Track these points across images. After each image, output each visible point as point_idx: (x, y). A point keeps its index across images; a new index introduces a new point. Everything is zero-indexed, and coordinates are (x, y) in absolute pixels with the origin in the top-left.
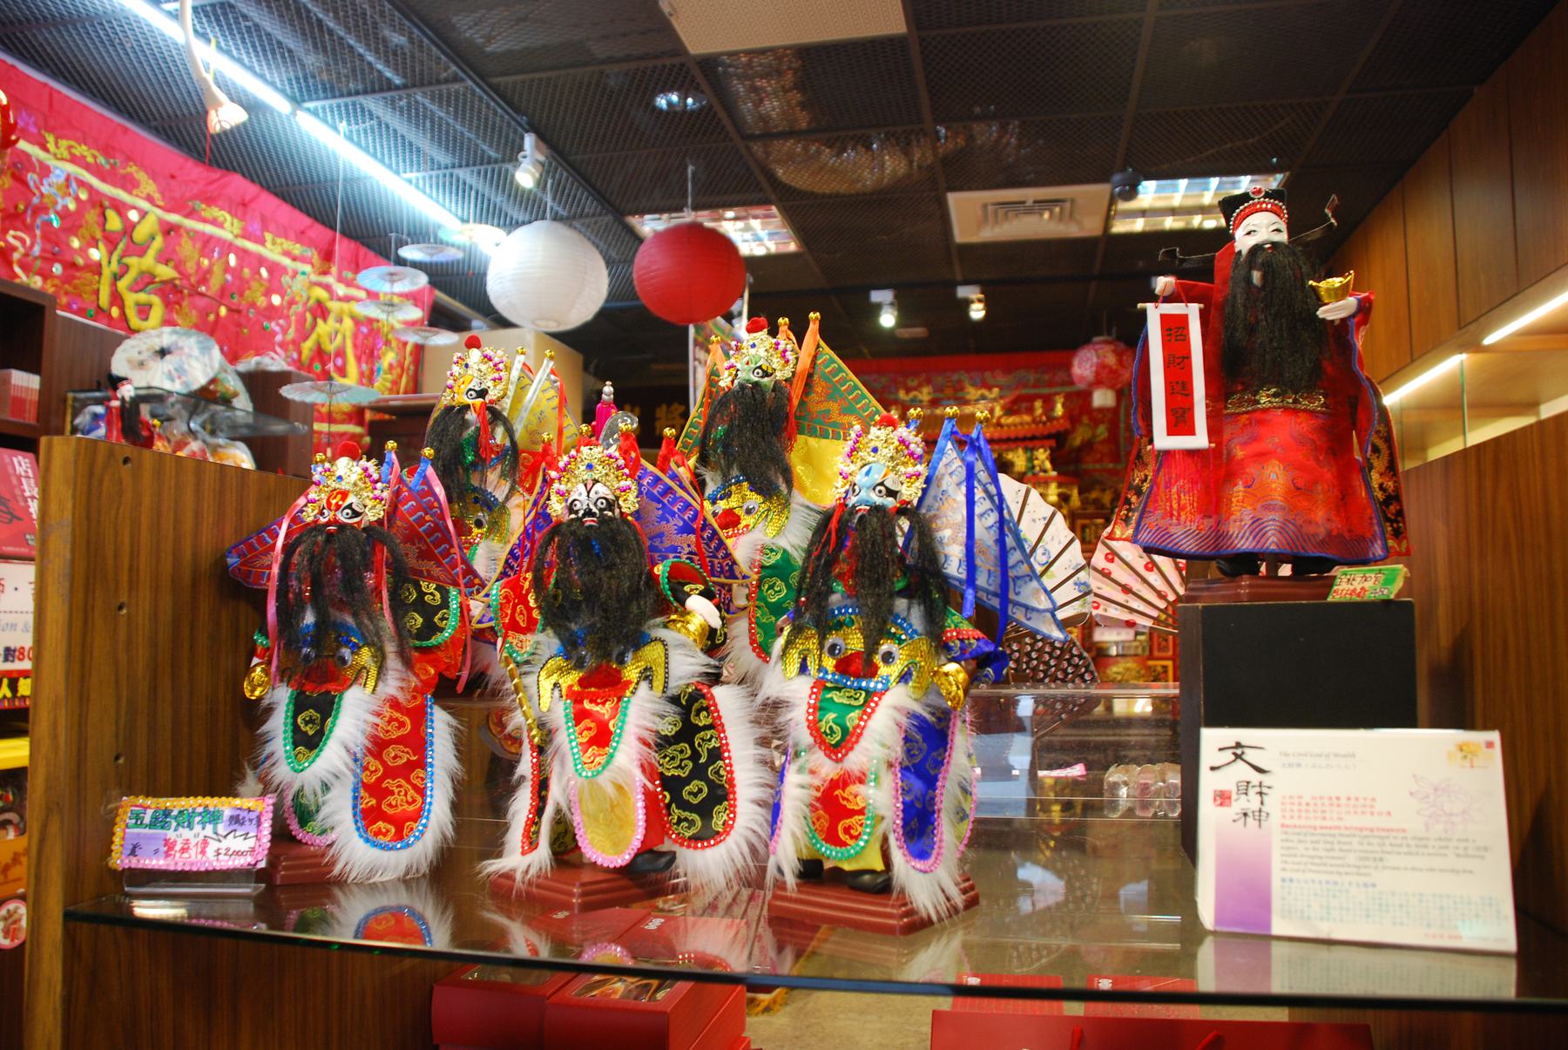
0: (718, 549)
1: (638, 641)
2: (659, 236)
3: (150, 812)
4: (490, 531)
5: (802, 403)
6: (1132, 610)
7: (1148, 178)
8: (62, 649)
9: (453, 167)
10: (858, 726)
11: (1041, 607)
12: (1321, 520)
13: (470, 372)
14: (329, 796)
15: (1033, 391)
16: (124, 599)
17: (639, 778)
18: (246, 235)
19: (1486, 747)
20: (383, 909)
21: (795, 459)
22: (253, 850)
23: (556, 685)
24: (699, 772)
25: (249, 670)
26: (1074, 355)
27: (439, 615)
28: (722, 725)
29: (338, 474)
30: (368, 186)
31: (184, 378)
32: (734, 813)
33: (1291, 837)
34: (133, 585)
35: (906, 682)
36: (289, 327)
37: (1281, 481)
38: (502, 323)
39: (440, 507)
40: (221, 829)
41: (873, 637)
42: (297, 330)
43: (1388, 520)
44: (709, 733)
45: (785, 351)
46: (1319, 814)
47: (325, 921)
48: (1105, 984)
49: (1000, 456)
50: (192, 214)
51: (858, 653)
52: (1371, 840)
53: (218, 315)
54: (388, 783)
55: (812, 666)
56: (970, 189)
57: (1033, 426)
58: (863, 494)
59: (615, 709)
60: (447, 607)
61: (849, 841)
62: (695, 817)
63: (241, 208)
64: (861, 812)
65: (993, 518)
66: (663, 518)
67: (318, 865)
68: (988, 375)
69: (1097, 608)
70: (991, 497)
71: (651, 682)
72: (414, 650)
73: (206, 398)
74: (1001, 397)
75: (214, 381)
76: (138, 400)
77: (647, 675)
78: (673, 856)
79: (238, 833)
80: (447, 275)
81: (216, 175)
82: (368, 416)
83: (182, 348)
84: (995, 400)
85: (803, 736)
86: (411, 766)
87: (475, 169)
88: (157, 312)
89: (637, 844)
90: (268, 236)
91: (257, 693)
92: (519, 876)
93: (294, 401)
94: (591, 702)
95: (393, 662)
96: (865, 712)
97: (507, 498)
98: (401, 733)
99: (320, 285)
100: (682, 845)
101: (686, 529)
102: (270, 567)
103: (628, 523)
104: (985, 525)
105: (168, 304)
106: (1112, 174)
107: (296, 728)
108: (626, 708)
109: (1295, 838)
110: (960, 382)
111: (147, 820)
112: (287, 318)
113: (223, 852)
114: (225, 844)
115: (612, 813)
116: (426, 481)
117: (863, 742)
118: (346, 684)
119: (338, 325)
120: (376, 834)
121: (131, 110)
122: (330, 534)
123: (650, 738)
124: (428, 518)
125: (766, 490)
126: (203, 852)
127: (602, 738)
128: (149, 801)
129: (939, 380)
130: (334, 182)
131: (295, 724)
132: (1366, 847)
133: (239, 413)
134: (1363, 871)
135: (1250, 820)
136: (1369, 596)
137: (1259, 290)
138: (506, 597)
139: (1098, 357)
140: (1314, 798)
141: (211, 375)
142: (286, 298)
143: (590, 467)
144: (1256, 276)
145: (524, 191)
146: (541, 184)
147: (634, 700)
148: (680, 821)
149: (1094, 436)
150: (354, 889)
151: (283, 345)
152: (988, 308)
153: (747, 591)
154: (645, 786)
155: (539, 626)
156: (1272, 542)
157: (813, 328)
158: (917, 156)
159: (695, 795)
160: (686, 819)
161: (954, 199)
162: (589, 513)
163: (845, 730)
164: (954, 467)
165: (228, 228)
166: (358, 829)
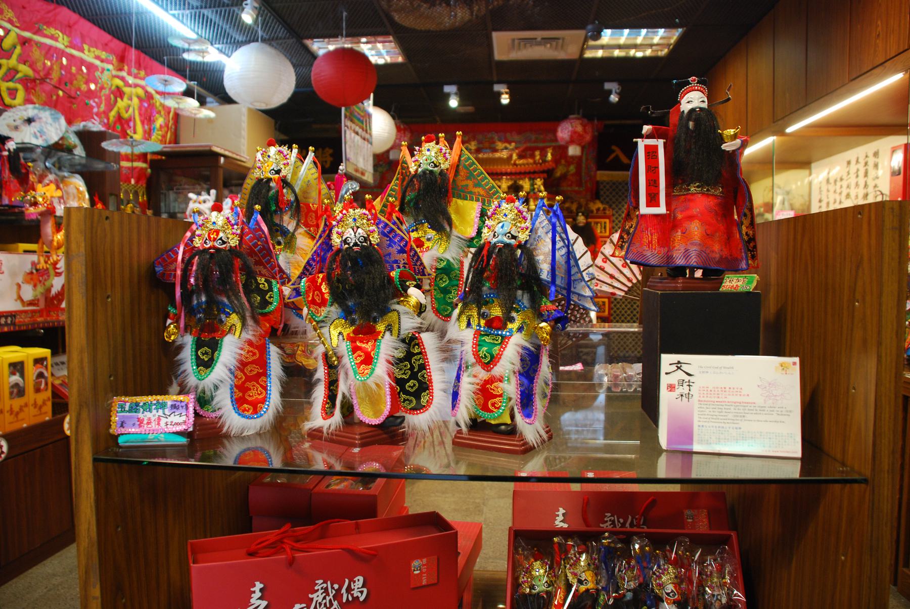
0: (417, 261)
1: (385, 311)
2: (330, 54)
3: (128, 404)
4: (285, 247)
5: (454, 180)
6: (614, 287)
7: (607, 28)
8: (83, 322)
9: (201, 8)
10: (499, 354)
11: (587, 295)
12: (717, 249)
13: (271, 160)
14: (218, 392)
15: (533, 145)
16: (109, 293)
17: (387, 378)
18: (72, 46)
19: (792, 363)
20: (249, 449)
21: (451, 210)
22: (185, 422)
23: (340, 333)
24: (414, 376)
25: (165, 328)
26: (558, 125)
27: (268, 295)
28: (425, 352)
29: (213, 221)
30: (148, 17)
31: (44, 137)
32: (432, 396)
33: (702, 406)
34: (113, 285)
35: (521, 332)
36: (101, 103)
37: (700, 230)
38: (226, 99)
39: (266, 237)
40: (167, 412)
41: (508, 310)
42: (106, 105)
43: (749, 250)
44: (419, 356)
45: (445, 153)
46: (716, 395)
47: (217, 456)
48: (591, 475)
49: (515, 182)
50: (38, 32)
51: (497, 317)
52: (740, 408)
53: (58, 96)
54: (248, 384)
55: (474, 323)
56: (506, 30)
57: (535, 166)
58: (500, 237)
59: (374, 346)
60: (272, 291)
61: (495, 410)
62: (412, 398)
63: (68, 29)
64: (501, 396)
65: (564, 251)
66: (390, 245)
67: (215, 428)
68: (508, 135)
69: (596, 286)
70: (563, 240)
71: (391, 332)
72: (259, 314)
73: (59, 148)
74: (516, 148)
75: (62, 138)
76: (18, 150)
77: (389, 328)
78: (403, 419)
79: (176, 414)
80: (197, 71)
81: (52, 7)
82: (149, 157)
83: (40, 118)
84: (513, 150)
85: (471, 359)
86: (259, 375)
87: (215, 10)
88: (21, 94)
89: (387, 413)
90: (86, 47)
91: (172, 338)
92: (325, 430)
93: (108, 150)
94: (360, 342)
95: (250, 322)
96: (502, 347)
97: (295, 230)
98: (255, 358)
99: (118, 77)
100: (406, 413)
101: (402, 251)
102: (175, 270)
103: (374, 248)
104: (561, 253)
105: (27, 89)
106: (587, 24)
107: (197, 357)
108: (379, 346)
109: (705, 406)
110: (492, 138)
111: (127, 408)
112: (100, 98)
113: (169, 423)
114: (170, 419)
115: (373, 399)
116: (257, 223)
117: (502, 362)
118: (224, 334)
119: (130, 102)
120: (244, 410)
121: (81, 12)
122: (212, 254)
123: (391, 359)
124: (259, 243)
125: (437, 227)
126: (159, 424)
127: (368, 360)
128: (127, 399)
129: (480, 137)
130: (131, 14)
131: (197, 355)
132: (737, 411)
133: (77, 157)
134: (735, 422)
135: (684, 398)
136: (740, 289)
137: (692, 132)
138: (309, 287)
139: (572, 127)
140: (714, 388)
141: (61, 135)
142: (99, 85)
143: (355, 220)
144: (691, 124)
145: (247, 25)
146: (256, 21)
147: (383, 341)
148: (405, 400)
149: (568, 171)
150: (234, 439)
151: (98, 114)
152: (511, 98)
153: (429, 281)
154: (390, 384)
155: (329, 303)
156: (693, 261)
157: (458, 140)
158: (476, 8)
159: (412, 387)
160: (408, 400)
161: (496, 36)
162: (356, 244)
163: (492, 357)
164: (544, 224)
165: (62, 42)
166: (234, 409)
